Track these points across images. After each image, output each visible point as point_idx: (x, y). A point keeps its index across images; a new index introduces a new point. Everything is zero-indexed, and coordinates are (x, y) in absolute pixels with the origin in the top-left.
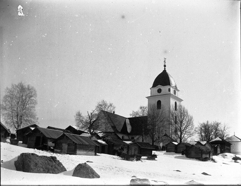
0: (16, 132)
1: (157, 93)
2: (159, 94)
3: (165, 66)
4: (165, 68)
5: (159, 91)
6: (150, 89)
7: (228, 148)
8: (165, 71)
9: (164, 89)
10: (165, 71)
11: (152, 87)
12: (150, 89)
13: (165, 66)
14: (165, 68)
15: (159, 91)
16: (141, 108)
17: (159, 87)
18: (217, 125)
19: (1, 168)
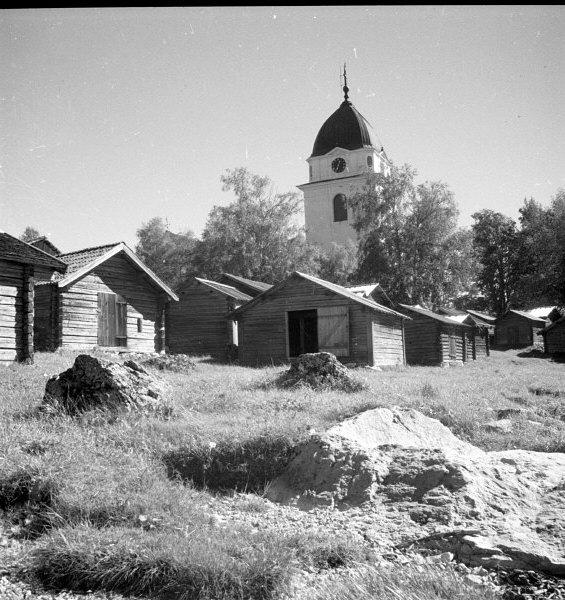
0: (475, 227)
1: (330, 173)
2: (337, 175)
3: (346, 90)
4: (346, 97)
5: (339, 165)
6: (308, 161)
7: (302, 345)
8: (346, 105)
9: (352, 158)
10: (346, 105)
11: (312, 156)
12: (308, 161)
13: (346, 90)
14: (346, 97)
15: (339, 165)
16: (520, 210)
17: (338, 152)
18: (156, 222)
19: (562, 388)
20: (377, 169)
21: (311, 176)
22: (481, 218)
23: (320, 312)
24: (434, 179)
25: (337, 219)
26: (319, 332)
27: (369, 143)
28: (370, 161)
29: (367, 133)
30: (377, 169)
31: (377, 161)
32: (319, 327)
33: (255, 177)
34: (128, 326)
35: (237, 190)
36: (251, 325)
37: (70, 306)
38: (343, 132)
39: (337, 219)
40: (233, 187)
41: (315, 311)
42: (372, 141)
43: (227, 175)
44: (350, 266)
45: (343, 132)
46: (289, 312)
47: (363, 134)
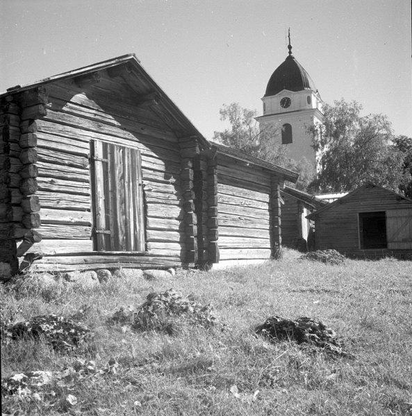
1: (280, 109)
2: (285, 110)
3: (290, 47)
4: (290, 53)
5: (286, 103)
6: (262, 99)
8: (290, 59)
9: (296, 97)
10: (290, 59)
11: (265, 96)
12: (262, 99)
13: (290, 47)
14: (290, 53)
15: (286, 103)
17: (285, 93)
20: (314, 106)
21: (264, 110)
22: (398, 142)
23: (388, 213)
24: (377, 112)
25: (284, 142)
26: (388, 230)
27: (308, 86)
28: (309, 100)
29: (307, 80)
30: (314, 106)
31: (314, 100)
32: (388, 225)
33: (245, 110)
34: (268, 227)
35: (232, 119)
36: (326, 224)
37: (264, 214)
38: (288, 78)
39: (284, 142)
40: (228, 118)
41: (384, 213)
42: (311, 84)
43: (223, 108)
44: (306, 177)
45: (288, 78)
46: (360, 214)
47: (304, 80)
